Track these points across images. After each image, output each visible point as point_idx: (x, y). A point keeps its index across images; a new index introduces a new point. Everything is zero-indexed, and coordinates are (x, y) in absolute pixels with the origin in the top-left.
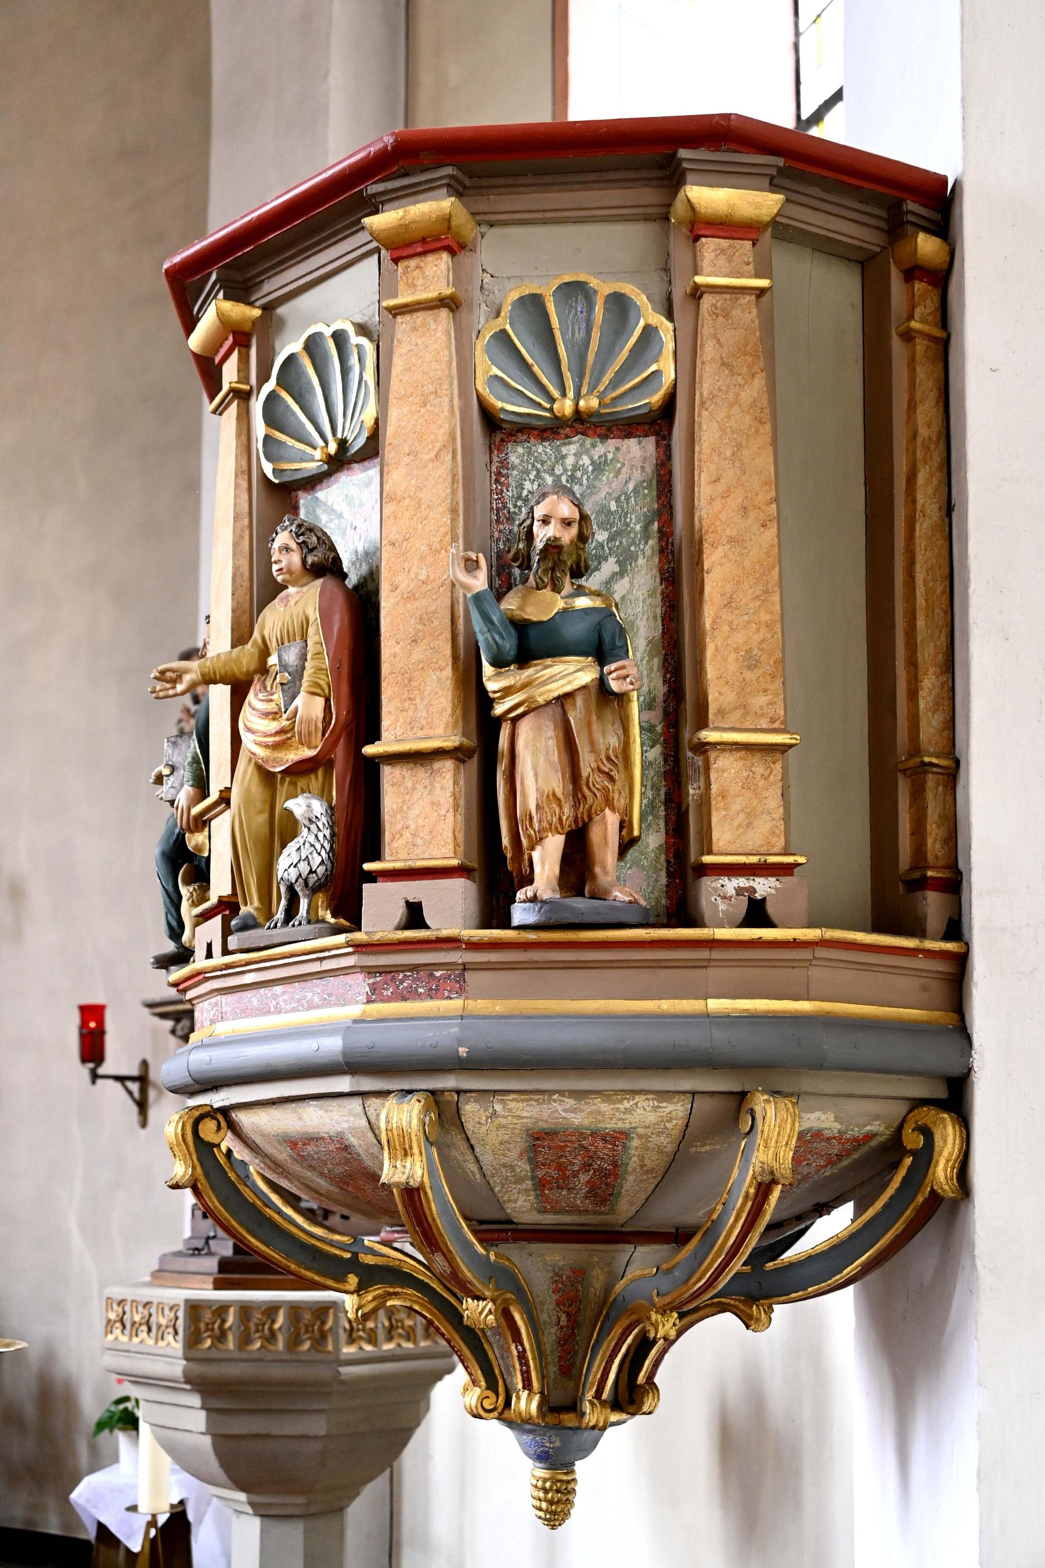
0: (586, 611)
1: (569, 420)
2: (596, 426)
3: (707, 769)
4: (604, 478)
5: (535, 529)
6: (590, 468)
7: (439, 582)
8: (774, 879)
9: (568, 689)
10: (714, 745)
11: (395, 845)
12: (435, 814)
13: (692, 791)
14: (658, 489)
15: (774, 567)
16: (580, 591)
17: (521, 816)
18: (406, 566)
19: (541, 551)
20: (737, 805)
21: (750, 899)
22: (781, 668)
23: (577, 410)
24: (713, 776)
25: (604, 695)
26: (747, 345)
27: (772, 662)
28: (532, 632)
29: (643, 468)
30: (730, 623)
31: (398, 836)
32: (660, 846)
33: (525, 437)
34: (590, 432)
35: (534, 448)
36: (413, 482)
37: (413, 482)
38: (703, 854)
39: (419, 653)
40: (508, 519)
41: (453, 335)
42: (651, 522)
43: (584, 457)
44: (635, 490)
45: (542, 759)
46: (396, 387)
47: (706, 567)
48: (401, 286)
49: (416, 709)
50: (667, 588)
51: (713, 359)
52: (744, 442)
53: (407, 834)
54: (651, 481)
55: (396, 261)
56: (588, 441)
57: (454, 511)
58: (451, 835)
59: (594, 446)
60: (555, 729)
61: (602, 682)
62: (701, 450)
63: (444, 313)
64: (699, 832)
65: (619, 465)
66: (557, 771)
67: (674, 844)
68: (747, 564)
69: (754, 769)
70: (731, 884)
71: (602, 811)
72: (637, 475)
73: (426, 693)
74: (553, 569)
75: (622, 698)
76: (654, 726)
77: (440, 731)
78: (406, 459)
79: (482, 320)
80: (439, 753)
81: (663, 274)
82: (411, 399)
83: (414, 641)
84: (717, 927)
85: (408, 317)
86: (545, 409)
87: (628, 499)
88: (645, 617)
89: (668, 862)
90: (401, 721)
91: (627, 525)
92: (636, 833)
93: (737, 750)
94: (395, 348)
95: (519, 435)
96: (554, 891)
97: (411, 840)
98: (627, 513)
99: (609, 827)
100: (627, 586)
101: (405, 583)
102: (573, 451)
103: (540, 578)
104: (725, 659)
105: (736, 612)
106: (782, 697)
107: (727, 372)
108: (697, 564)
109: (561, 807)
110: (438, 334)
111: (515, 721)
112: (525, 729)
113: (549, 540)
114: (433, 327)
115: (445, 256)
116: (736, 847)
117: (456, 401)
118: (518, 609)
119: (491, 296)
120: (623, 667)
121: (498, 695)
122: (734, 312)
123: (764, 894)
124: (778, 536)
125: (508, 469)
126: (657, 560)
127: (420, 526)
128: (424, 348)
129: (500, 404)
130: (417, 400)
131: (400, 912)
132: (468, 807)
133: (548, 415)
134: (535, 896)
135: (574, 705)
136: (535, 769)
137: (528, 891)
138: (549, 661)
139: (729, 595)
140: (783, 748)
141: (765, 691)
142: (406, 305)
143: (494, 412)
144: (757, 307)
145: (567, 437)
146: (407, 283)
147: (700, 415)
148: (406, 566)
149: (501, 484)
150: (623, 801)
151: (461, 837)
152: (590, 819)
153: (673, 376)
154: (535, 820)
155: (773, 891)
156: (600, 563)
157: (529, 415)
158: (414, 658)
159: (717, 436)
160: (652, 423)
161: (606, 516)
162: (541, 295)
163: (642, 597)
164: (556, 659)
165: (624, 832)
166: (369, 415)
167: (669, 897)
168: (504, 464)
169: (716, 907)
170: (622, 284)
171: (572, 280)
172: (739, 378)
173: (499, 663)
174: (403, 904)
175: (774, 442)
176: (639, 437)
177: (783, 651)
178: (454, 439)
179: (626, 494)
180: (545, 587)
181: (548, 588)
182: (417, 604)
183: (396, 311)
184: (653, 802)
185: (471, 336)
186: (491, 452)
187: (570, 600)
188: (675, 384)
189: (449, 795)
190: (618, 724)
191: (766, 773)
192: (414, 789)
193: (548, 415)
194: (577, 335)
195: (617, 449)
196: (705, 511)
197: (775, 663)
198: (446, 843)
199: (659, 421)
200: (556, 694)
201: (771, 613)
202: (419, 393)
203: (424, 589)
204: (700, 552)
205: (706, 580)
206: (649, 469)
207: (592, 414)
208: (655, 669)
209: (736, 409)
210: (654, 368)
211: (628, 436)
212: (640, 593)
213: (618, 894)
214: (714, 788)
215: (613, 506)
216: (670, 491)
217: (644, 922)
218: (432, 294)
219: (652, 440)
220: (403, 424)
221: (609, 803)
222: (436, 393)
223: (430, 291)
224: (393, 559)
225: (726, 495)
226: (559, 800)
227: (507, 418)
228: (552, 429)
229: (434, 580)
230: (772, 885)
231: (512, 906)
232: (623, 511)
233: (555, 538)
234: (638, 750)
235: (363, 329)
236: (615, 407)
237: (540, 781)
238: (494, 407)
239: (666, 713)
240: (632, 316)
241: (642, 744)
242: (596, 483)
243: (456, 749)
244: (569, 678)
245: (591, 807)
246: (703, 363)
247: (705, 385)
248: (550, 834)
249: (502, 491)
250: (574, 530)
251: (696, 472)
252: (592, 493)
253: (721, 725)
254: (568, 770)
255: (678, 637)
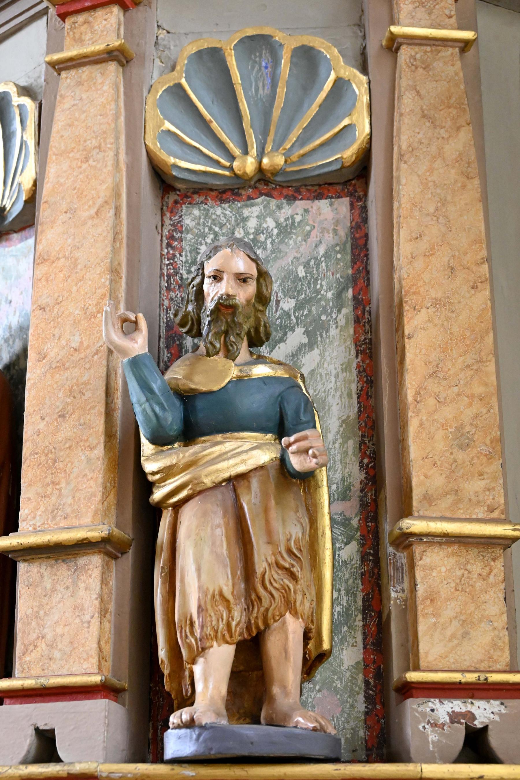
0: (265, 380)
1: (251, 179)
2: (282, 186)
3: (412, 566)
4: (291, 242)
5: (205, 287)
6: (276, 231)
7: (94, 350)
8: (498, 702)
9: (242, 469)
10: (420, 536)
11: (28, 659)
12: (77, 620)
13: (394, 594)
14: (353, 254)
15: (487, 333)
16: (260, 359)
17: (180, 621)
18: (57, 332)
19: (212, 312)
20: (449, 611)
21: (467, 727)
22: (499, 448)
23: (260, 170)
24: (419, 575)
25: (288, 479)
26: (450, 97)
27: (488, 441)
28: (200, 404)
29: (335, 231)
30: (437, 397)
31: (31, 647)
32: (358, 663)
33: (202, 198)
34: (275, 193)
35: (212, 210)
36: (69, 241)
37: (69, 241)
38: (408, 670)
39: (66, 430)
40: (180, 286)
41: (122, 89)
42: (344, 289)
43: (268, 219)
44: (326, 255)
45: (207, 551)
46: (56, 142)
47: (407, 332)
48: (68, 41)
49: (60, 495)
50: (363, 361)
51: (412, 111)
52: (449, 198)
53: (43, 645)
54: (345, 244)
55: (63, 17)
56: (273, 203)
57: (114, 271)
58: (95, 645)
59: (279, 207)
60: (224, 516)
61: (283, 462)
62: (400, 205)
63: (112, 67)
64: (404, 645)
65: (308, 228)
66: (225, 566)
67: (374, 662)
68: (455, 329)
69: (469, 567)
70: (444, 709)
71: (282, 616)
72: (329, 239)
73: (72, 476)
74: (226, 333)
75: (307, 478)
76: (349, 519)
77: (87, 520)
78: (63, 217)
79: (156, 74)
80: (83, 546)
81: (356, 29)
82: (71, 155)
83: (62, 416)
84: (426, 762)
85: (73, 72)
86: (224, 167)
87: (318, 265)
88: (338, 394)
89: (367, 683)
90: (42, 508)
91: (318, 292)
92: (326, 646)
93: (448, 543)
94: (57, 103)
95: (196, 196)
96: (218, 714)
97: (46, 652)
98: (317, 280)
99: (291, 637)
100: (318, 359)
101: (54, 351)
102: (256, 214)
103: (211, 343)
104: (431, 438)
105: (444, 383)
106: (501, 482)
107: (428, 124)
108: (397, 331)
109: (229, 610)
110: (105, 88)
111: (177, 507)
112: (188, 516)
113: (220, 298)
114: (100, 80)
115: (116, 10)
116: (450, 661)
117: (122, 157)
118: (185, 377)
119: (167, 52)
120: (305, 438)
121: (157, 477)
122: (435, 64)
123: (486, 721)
124: (492, 300)
125: (181, 232)
126: (352, 331)
127: (75, 289)
128: (91, 103)
129: (172, 160)
130: (78, 156)
131: (28, 742)
132: (118, 614)
133: (227, 173)
134: (192, 720)
135: (249, 488)
136: (199, 563)
137: (185, 714)
138: (219, 437)
139: (434, 364)
140: (506, 543)
141: (481, 474)
142: (71, 59)
143: (165, 169)
144: (461, 58)
145: (249, 198)
146: (74, 39)
147: (398, 169)
148: (57, 332)
149: (173, 248)
150: (307, 605)
151: (108, 649)
152: (267, 626)
153: (367, 130)
154: (197, 625)
155: (497, 718)
156: (285, 334)
157: (205, 173)
158: (61, 436)
159: (418, 190)
160: (346, 183)
161: (293, 282)
162: (220, 49)
163: (334, 372)
164: (228, 435)
165: (311, 645)
166: (26, 179)
167: (368, 728)
168: (178, 227)
169: (424, 737)
170: (310, 38)
171: (255, 33)
172: (442, 131)
173: (160, 440)
174: (31, 731)
175: (484, 199)
176: (331, 198)
177: (501, 428)
178: (118, 195)
179: (316, 259)
180: (217, 353)
181: (221, 354)
182: (67, 374)
183: (59, 67)
184: (347, 609)
185: (142, 90)
186: (163, 215)
187: (246, 368)
188: (371, 139)
189: (94, 596)
190: (302, 513)
191: (485, 573)
192: (53, 590)
193: (227, 173)
194: (261, 91)
195: (306, 211)
196: (405, 270)
197: (491, 442)
198: (89, 656)
199: (354, 179)
200: (226, 475)
201: (486, 385)
202: (81, 148)
203: (76, 357)
204: (401, 315)
205: (407, 347)
206: (343, 232)
207: (276, 173)
208: (350, 452)
209: (438, 163)
210: (346, 122)
211: (319, 197)
212: (332, 367)
213: (300, 719)
214: (421, 589)
215: (301, 272)
216: (367, 256)
217: (333, 756)
218: (100, 46)
219: (346, 201)
220: (62, 180)
221: (290, 606)
222: (99, 147)
223: (99, 44)
224: (42, 325)
225: (429, 254)
226: (228, 601)
227: (180, 176)
228: (232, 190)
229: (88, 347)
230: (496, 710)
231: (165, 734)
232: (312, 277)
233: (228, 295)
234: (328, 544)
235: (26, 91)
236: (303, 164)
237: (203, 576)
238: (166, 164)
239: (363, 505)
240: (322, 70)
241: (334, 540)
242: (282, 247)
243: (105, 541)
244: (244, 457)
245: (267, 610)
246: (401, 115)
247: (404, 138)
248: (215, 644)
249: (174, 256)
250: (251, 288)
251: (395, 231)
252: (276, 258)
253: (428, 513)
254: (240, 565)
255: (376, 415)
